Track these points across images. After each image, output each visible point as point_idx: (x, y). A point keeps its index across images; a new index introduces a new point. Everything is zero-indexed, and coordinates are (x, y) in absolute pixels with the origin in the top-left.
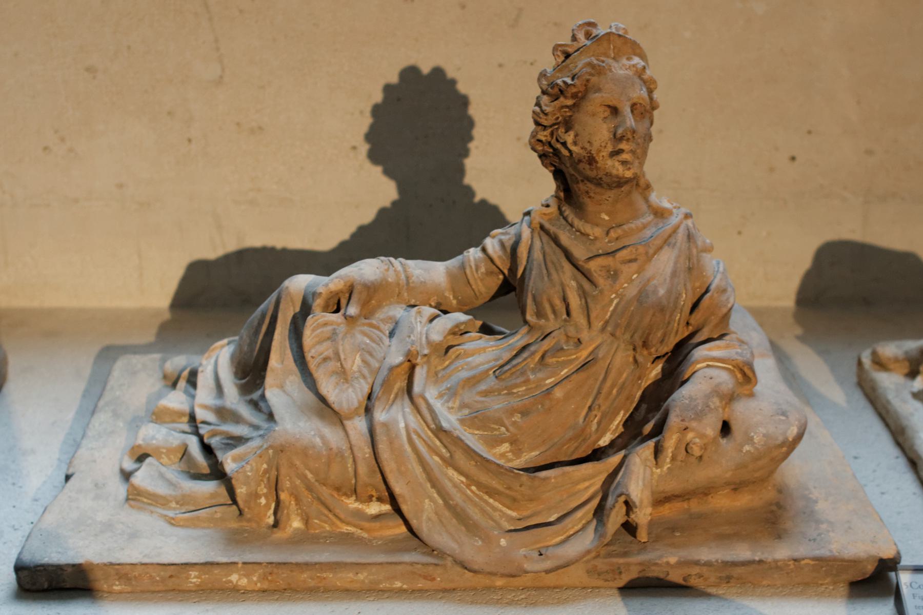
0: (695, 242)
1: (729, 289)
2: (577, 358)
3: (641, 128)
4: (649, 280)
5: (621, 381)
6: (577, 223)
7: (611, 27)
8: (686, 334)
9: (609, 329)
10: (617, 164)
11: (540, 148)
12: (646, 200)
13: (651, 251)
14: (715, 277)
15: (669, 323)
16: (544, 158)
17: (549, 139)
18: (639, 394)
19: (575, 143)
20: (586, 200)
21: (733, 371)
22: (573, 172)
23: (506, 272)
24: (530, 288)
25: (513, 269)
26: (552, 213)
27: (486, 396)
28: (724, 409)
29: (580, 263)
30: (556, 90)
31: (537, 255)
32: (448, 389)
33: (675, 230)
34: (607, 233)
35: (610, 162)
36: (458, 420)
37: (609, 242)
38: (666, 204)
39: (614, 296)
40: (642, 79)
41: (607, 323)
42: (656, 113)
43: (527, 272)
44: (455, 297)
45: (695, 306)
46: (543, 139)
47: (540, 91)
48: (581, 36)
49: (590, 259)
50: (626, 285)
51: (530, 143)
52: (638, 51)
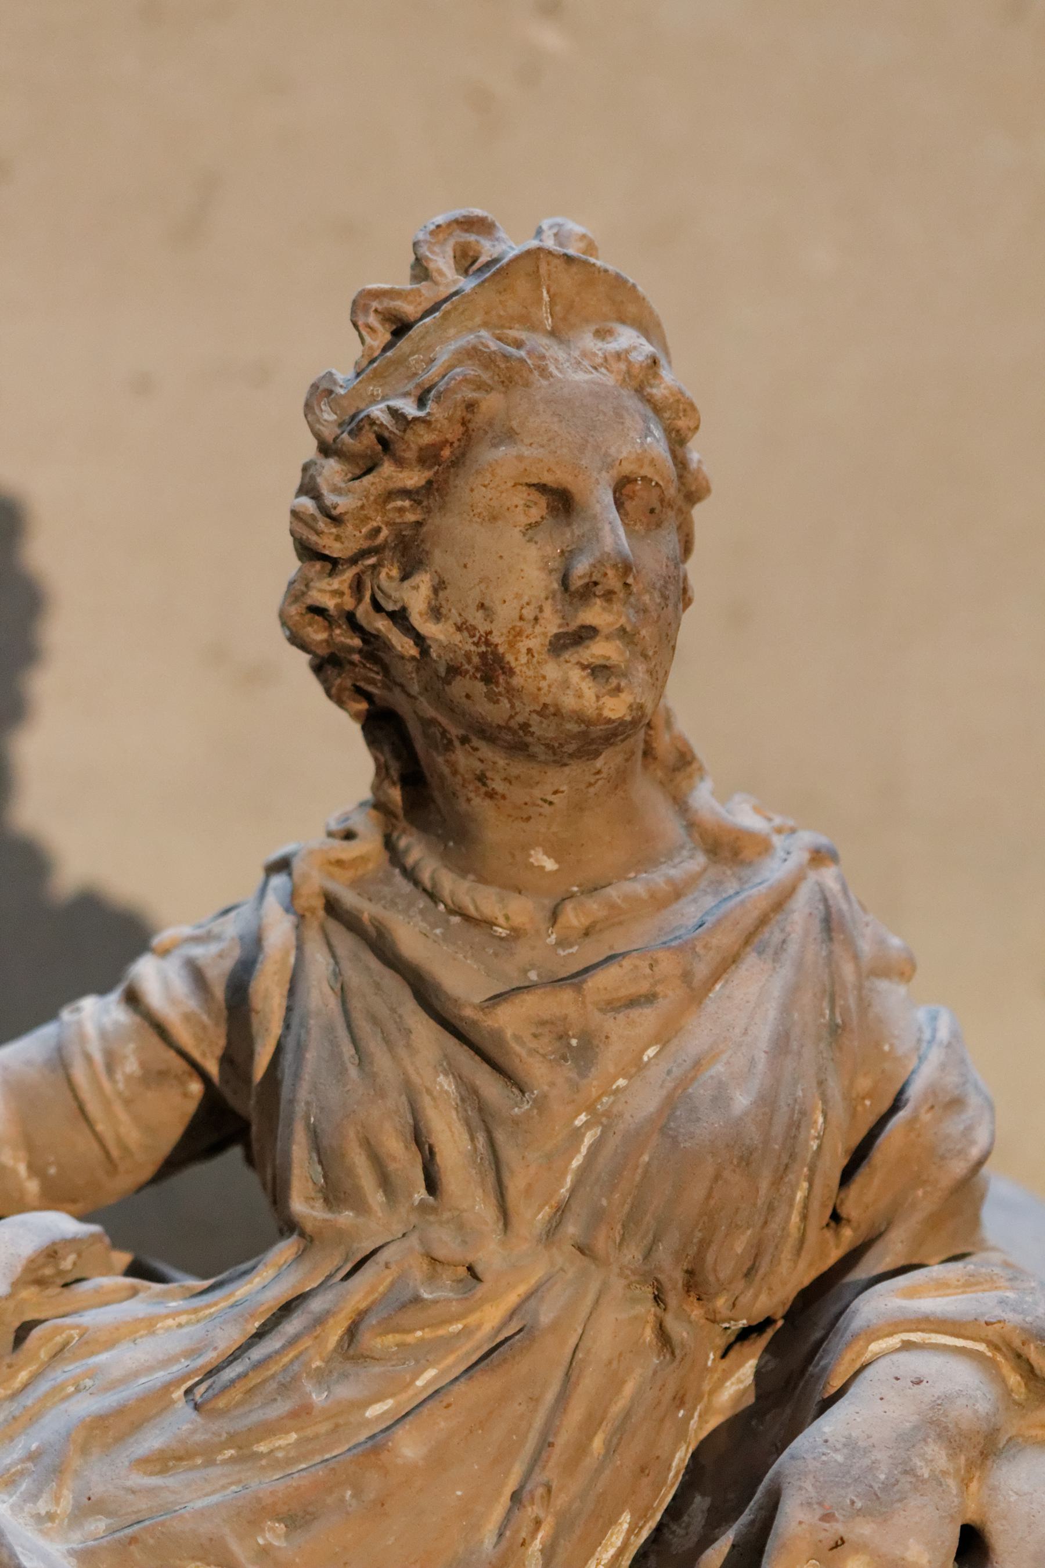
0: (850, 944)
1: (974, 1100)
2: (467, 1332)
3: (652, 557)
4: (697, 1065)
5: (617, 1407)
6: (449, 883)
7: (539, 232)
8: (834, 1255)
9: (571, 1229)
10: (576, 675)
11: (317, 635)
12: (681, 804)
13: (702, 970)
14: (921, 1059)
15: (771, 1208)
16: (330, 671)
17: (349, 603)
18: (681, 1457)
19: (436, 613)
20: (480, 805)
21: (992, 1360)
22: (431, 712)
23: (212, 1068)
24: (300, 1108)
25: (236, 1056)
26: (363, 859)
27: (164, 1471)
28: (965, 1483)
29: (468, 1012)
30: (368, 438)
31: (319, 995)
32: (33, 1457)
33: (781, 901)
34: (554, 916)
35: (552, 671)
36: (72, 1553)
37: (561, 943)
38: (746, 817)
39: (583, 1118)
40: (649, 400)
41: (562, 1211)
42: (699, 513)
43: (288, 1058)
44: (34, 1169)
45: (859, 1157)
46: (330, 603)
47: (314, 443)
48: (443, 263)
49: (497, 999)
50: (621, 1082)
51: (284, 620)
52: (632, 309)
